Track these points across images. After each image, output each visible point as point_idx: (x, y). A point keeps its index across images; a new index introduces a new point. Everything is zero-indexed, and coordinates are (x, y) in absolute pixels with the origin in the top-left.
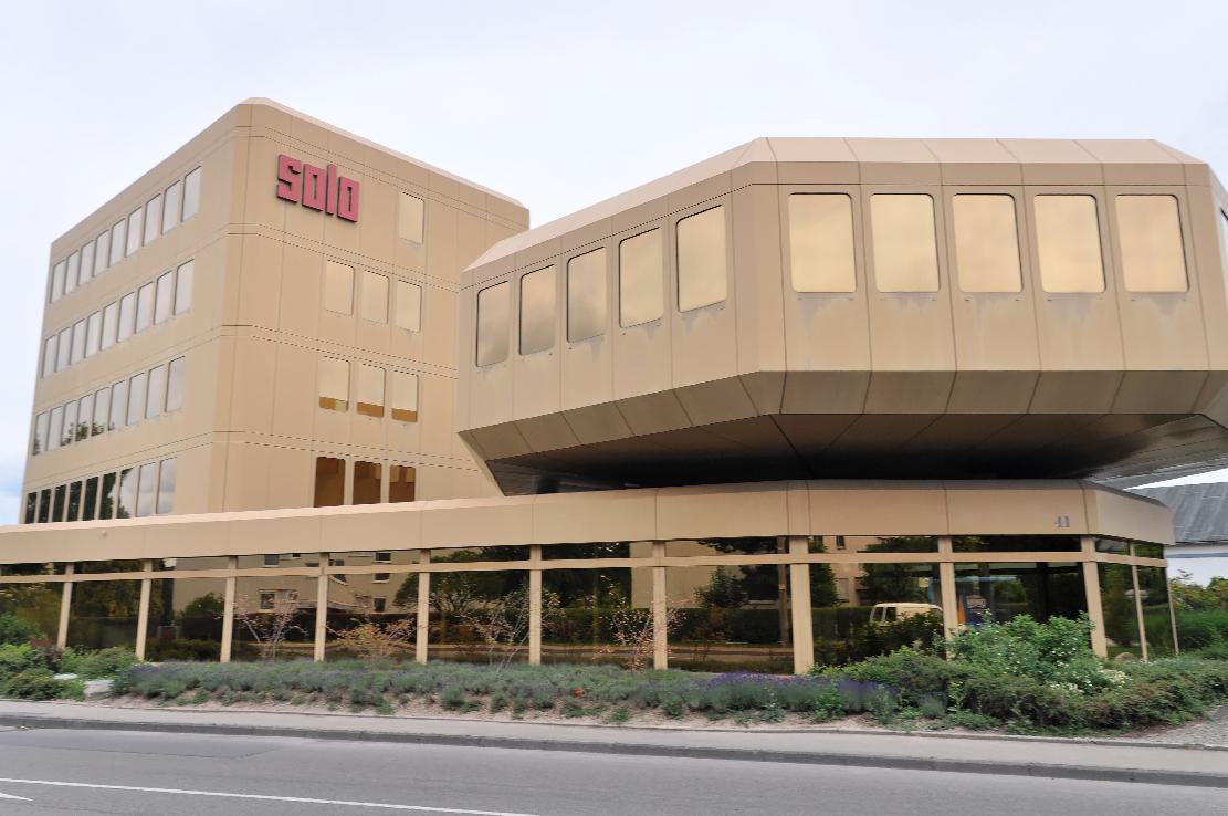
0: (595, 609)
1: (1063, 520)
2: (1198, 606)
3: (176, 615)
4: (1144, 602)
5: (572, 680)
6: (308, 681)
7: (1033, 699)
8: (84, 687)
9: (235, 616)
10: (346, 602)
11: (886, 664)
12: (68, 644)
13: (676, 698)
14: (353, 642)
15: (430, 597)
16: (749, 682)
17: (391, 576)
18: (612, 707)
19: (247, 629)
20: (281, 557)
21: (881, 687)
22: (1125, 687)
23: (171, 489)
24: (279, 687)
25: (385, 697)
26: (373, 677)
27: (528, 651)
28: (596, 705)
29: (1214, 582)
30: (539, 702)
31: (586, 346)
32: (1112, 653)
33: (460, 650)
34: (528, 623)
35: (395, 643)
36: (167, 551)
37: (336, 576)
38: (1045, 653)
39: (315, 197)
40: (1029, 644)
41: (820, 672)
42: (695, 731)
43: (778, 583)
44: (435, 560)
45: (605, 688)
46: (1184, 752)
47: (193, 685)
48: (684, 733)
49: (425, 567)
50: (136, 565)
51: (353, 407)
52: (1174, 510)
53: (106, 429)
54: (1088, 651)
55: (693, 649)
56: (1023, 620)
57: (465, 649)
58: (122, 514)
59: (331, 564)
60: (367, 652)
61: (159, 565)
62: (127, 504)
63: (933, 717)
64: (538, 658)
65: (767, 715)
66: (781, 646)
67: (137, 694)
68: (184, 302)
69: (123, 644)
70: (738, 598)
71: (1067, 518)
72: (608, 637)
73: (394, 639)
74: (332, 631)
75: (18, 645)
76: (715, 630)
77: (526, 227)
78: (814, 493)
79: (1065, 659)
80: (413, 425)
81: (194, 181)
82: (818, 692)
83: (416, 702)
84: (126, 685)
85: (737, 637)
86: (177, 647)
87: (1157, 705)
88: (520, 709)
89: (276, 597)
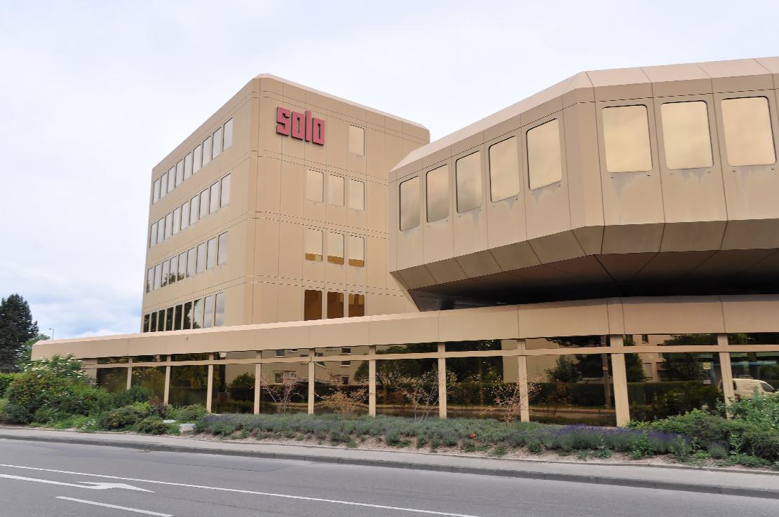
8: (179, 428)
9: (261, 387)
10: (325, 379)
13: (537, 441)
14: (331, 403)
16: (586, 432)
19: (268, 394)
21: (679, 436)
23: (222, 311)
24: (288, 430)
25: (351, 436)
26: (344, 424)
28: (484, 444)
30: (447, 441)
31: (469, 215)
34: (438, 391)
36: (223, 348)
37: (318, 362)
41: (636, 425)
42: (551, 463)
44: (378, 353)
45: (489, 433)
47: (239, 428)
49: (372, 358)
50: (204, 356)
51: (325, 258)
55: (546, 409)
58: (195, 326)
59: (315, 356)
61: (217, 356)
62: (199, 321)
63: (718, 458)
64: (445, 414)
65: (599, 454)
67: (208, 432)
68: (225, 200)
70: (575, 376)
72: (490, 401)
75: (143, 403)
76: (561, 397)
77: (428, 142)
81: (229, 126)
82: (634, 439)
83: (370, 440)
85: (576, 402)
86: (229, 405)
88: (435, 446)
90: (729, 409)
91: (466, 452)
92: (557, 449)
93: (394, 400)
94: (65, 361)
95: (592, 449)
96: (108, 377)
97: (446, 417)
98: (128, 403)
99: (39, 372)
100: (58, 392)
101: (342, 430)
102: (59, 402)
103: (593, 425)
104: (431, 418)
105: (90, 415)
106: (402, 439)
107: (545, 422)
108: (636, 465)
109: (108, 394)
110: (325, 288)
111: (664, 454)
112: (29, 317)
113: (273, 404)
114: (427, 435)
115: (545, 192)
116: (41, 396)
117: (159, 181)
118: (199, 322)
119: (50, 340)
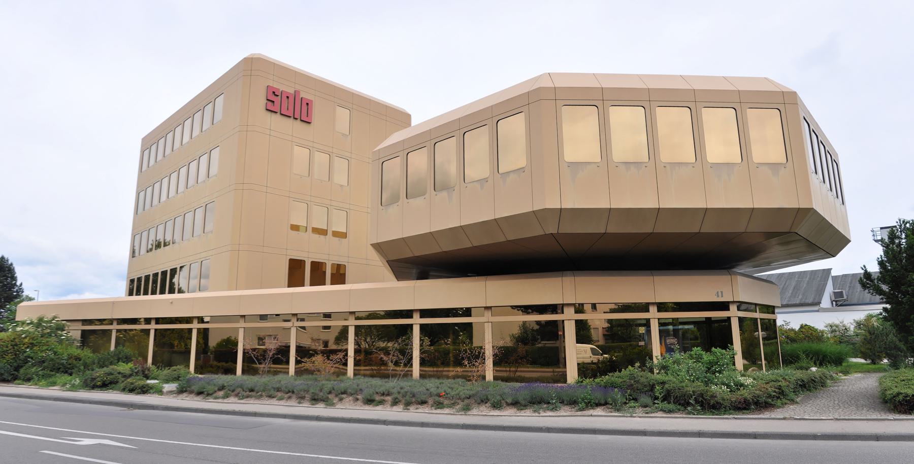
0: (451, 347)
1: (720, 294)
2: (793, 340)
3: (211, 348)
4: (764, 339)
5: (438, 388)
6: (286, 387)
7: (702, 395)
8: (163, 388)
9: (244, 350)
10: (307, 343)
11: (619, 377)
12: (153, 364)
13: (498, 398)
14: (311, 365)
15: (355, 340)
16: (541, 388)
17: (332, 327)
18: (462, 403)
19: (251, 357)
20: (269, 316)
21: (616, 390)
22: (752, 387)
23: (207, 277)
24: (270, 390)
25: (330, 396)
26: (323, 385)
27: (412, 371)
28: (452, 402)
29: (802, 327)
30: (419, 400)
31: (444, 194)
32: (746, 368)
33: (372, 370)
34: (412, 355)
35: (335, 366)
36: (206, 313)
37: (300, 327)
38: (709, 369)
39: (288, 109)
40: (700, 364)
41: (582, 382)
42: (509, 416)
43: (558, 331)
44: (357, 318)
45: (457, 392)
46: (783, 421)
47: (222, 388)
48: (503, 417)
49: (352, 323)
50: (188, 320)
51: (310, 230)
52: (782, 286)
53: (171, 242)
54: (733, 367)
55: (508, 369)
56: (697, 350)
57: (375, 370)
58: (180, 291)
59: (297, 321)
60: (319, 371)
61: (201, 320)
62: (183, 285)
63: (646, 406)
64: (418, 375)
65: (551, 407)
66: (560, 368)
67: (191, 392)
68: (214, 170)
69: (182, 364)
70: (535, 340)
71: (722, 292)
72: (458, 363)
73: (335, 364)
74: (299, 358)
75: (127, 363)
76: (521, 358)
77: (409, 125)
78: (578, 279)
79: (720, 372)
80: (343, 240)
81: (220, 101)
82: (581, 394)
83: (347, 400)
84: (184, 387)
85: (534, 363)
86: (212, 367)
87: (770, 396)
88: (408, 404)
89: (266, 338)
90: (656, 366)
91: (436, 409)
92: (516, 404)
93: (371, 362)
94: (50, 322)
95: (545, 403)
96: (92, 338)
97: (418, 378)
98: (111, 364)
99: (23, 332)
100: (42, 352)
101: (321, 390)
102: (44, 362)
103: (547, 383)
104: (405, 378)
105: (74, 375)
106: (378, 398)
107: (506, 381)
108: (581, 416)
109: (92, 355)
110: (308, 259)
111: (604, 405)
112: (14, 278)
113: (255, 366)
114: (401, 395)
115: (512, 176)
116: (25, 355)
117: (148, 150)
118: (184, 288)
119: (36, 301)
